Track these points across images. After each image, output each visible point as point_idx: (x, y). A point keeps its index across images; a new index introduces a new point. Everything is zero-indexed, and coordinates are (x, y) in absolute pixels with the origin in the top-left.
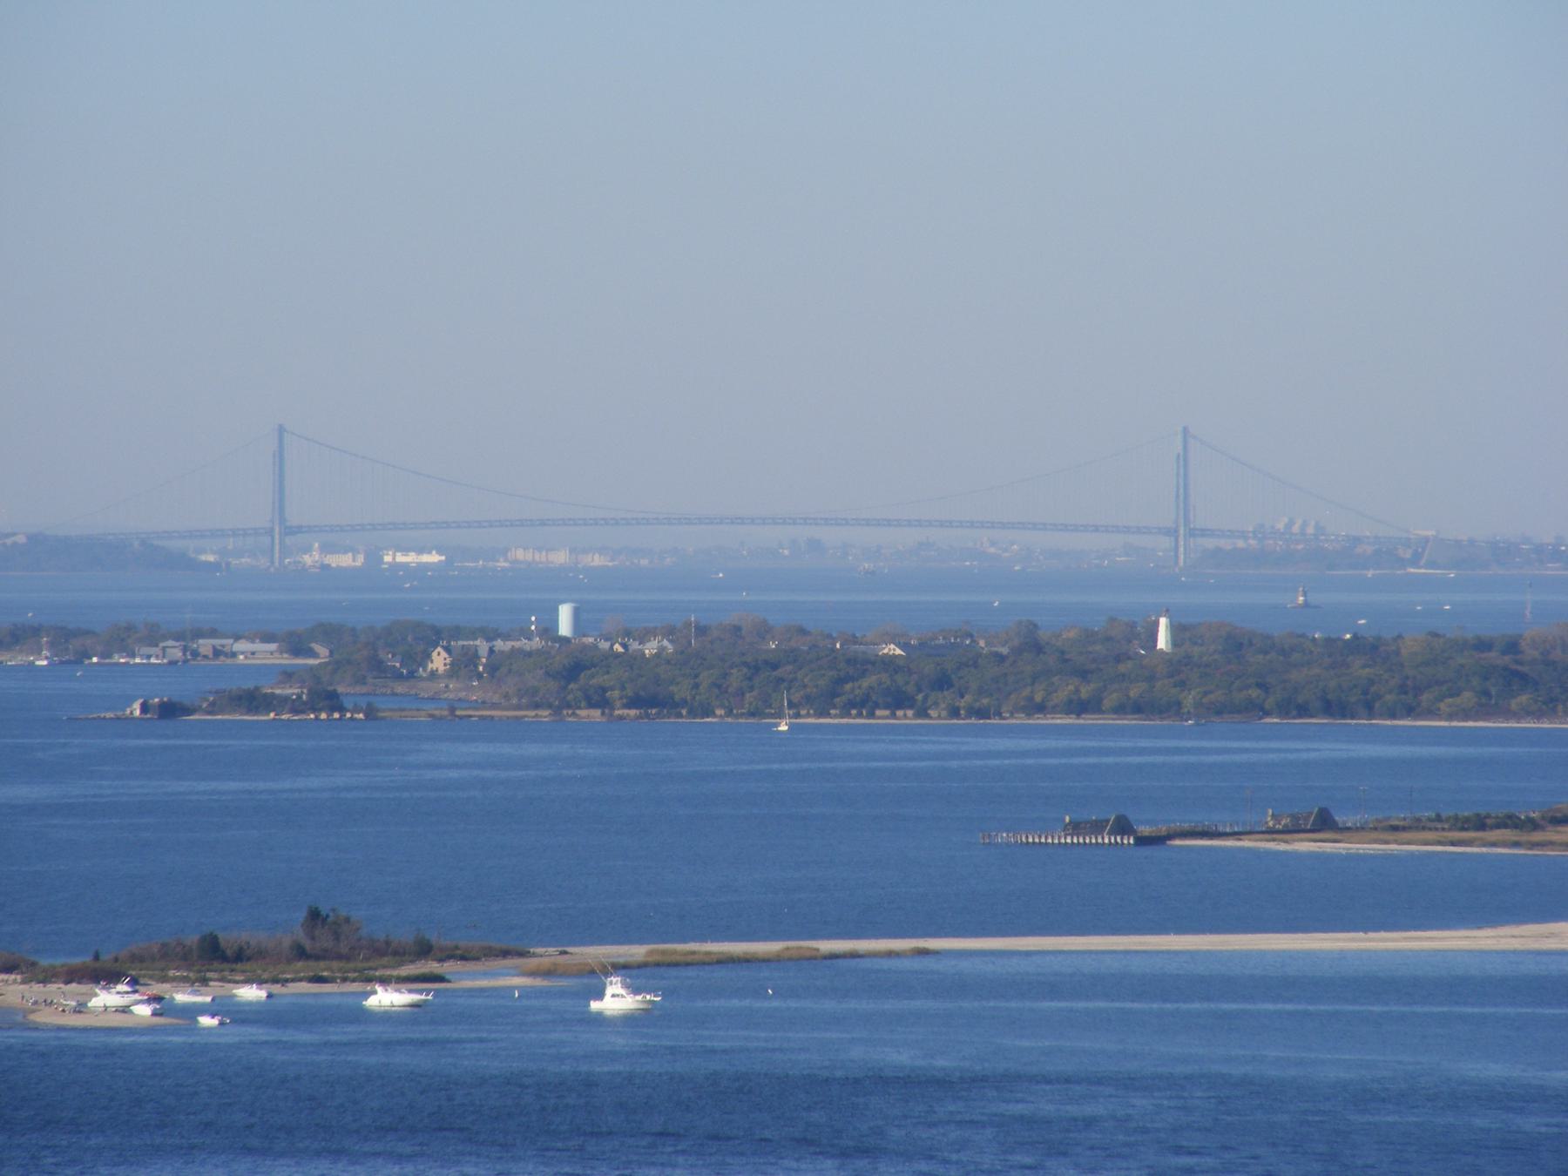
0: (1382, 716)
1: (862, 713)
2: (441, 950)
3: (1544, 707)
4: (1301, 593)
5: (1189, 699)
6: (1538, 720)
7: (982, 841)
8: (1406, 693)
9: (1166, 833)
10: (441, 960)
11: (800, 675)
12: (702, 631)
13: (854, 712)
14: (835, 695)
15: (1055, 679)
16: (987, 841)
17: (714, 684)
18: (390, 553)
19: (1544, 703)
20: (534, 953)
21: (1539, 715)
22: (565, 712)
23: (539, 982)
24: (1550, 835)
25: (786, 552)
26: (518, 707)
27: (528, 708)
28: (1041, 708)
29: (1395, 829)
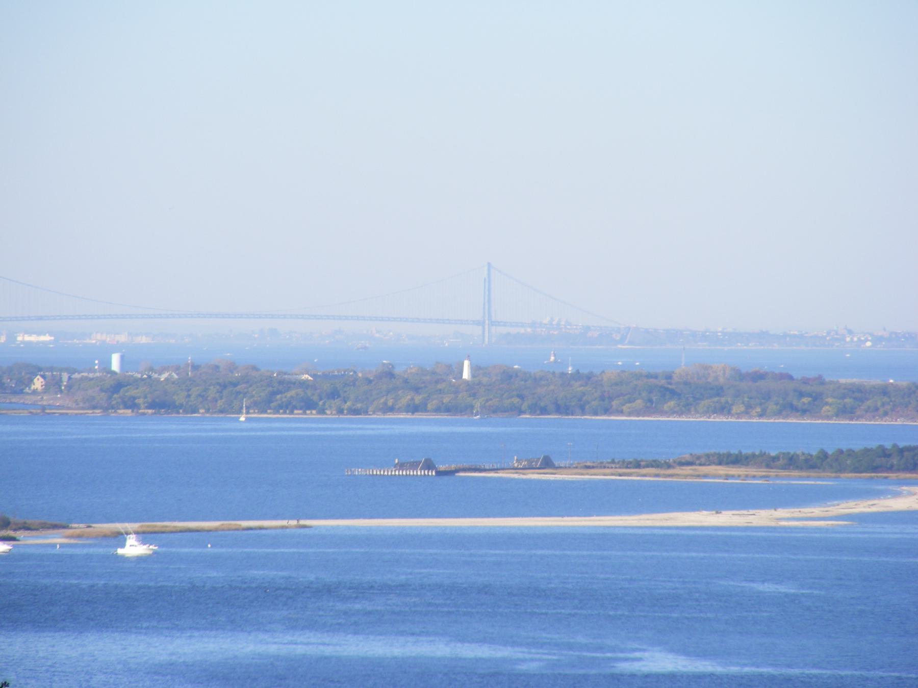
0: (589, 414)
1: (286, 412)
2: (16, 524)
3: (683, 408)
4: (552, 355)
5: (478, 404)
6: (680, 416)
7: (346, 473)
8: (604, 400)
9: (454, 469)
10: (15, 530)
11: (250, 389)
12: (195, 367)
13: (281, 411)
14: (270, 401)
15: (400, 392)
16: (350, 473)
17: (199, 395)
18: (21, 335)
19: (683, 406)
20: (71, 527)
21: (681, 414)
22: (110, 411)
23: (72, 541)
24: (678, 470)
25: (256, 336)
26: (83, 409)
27: (89, 409)
28: (391, 409)
29: (588, 467)
